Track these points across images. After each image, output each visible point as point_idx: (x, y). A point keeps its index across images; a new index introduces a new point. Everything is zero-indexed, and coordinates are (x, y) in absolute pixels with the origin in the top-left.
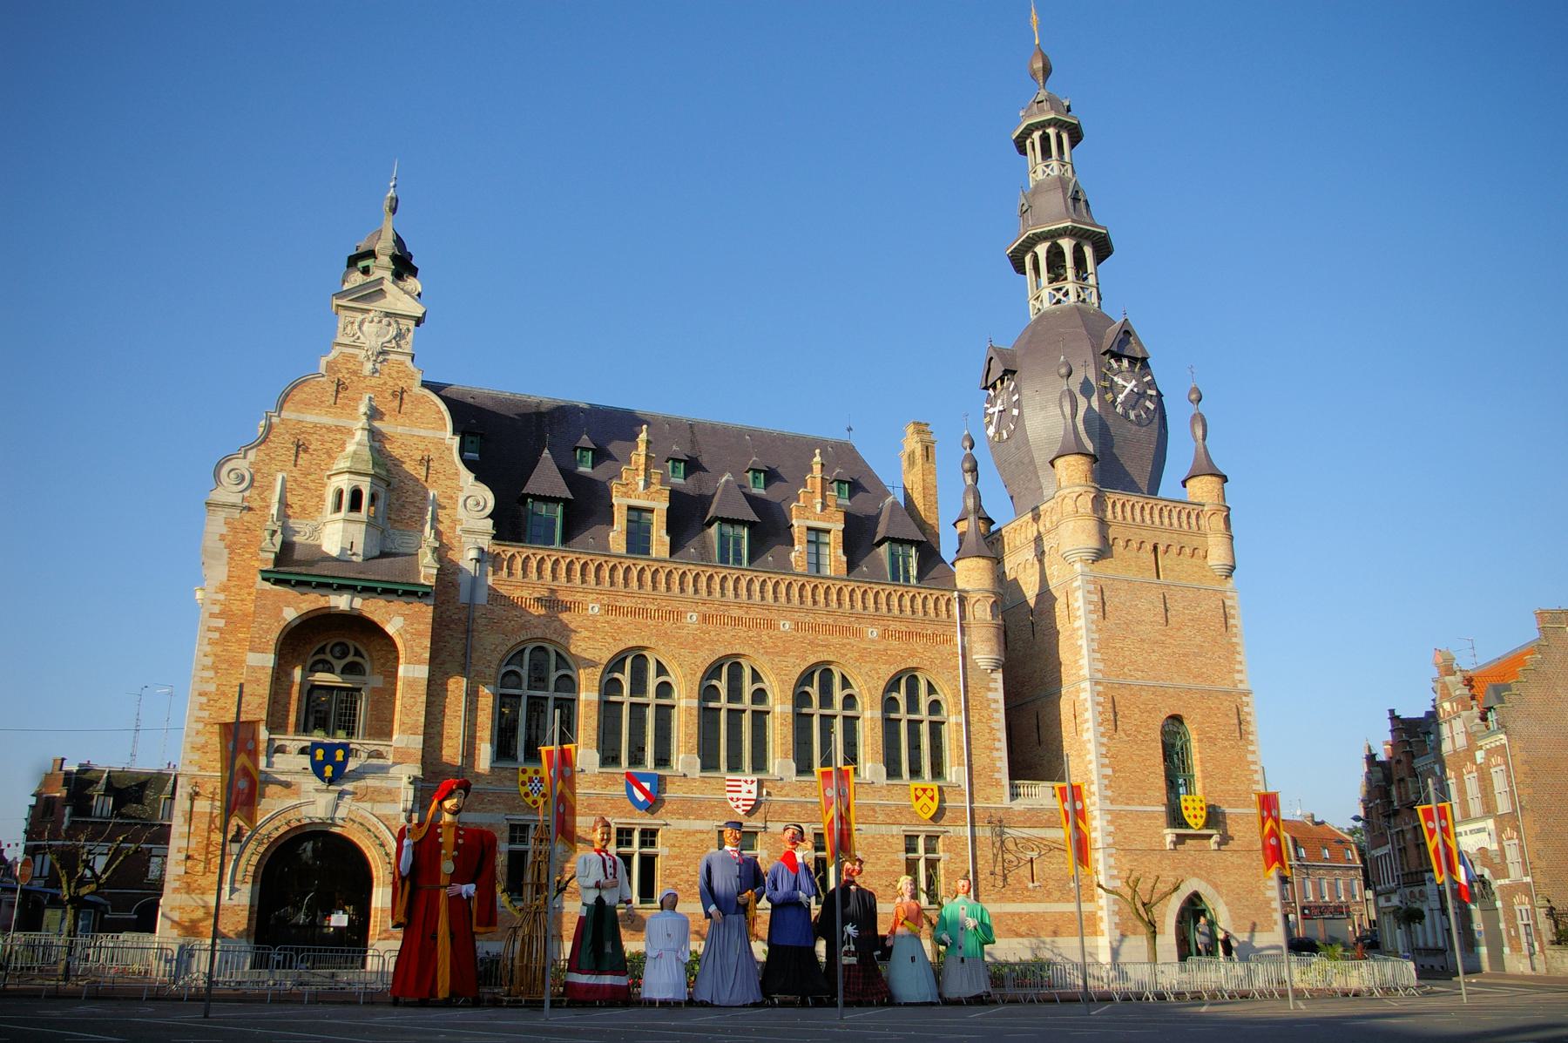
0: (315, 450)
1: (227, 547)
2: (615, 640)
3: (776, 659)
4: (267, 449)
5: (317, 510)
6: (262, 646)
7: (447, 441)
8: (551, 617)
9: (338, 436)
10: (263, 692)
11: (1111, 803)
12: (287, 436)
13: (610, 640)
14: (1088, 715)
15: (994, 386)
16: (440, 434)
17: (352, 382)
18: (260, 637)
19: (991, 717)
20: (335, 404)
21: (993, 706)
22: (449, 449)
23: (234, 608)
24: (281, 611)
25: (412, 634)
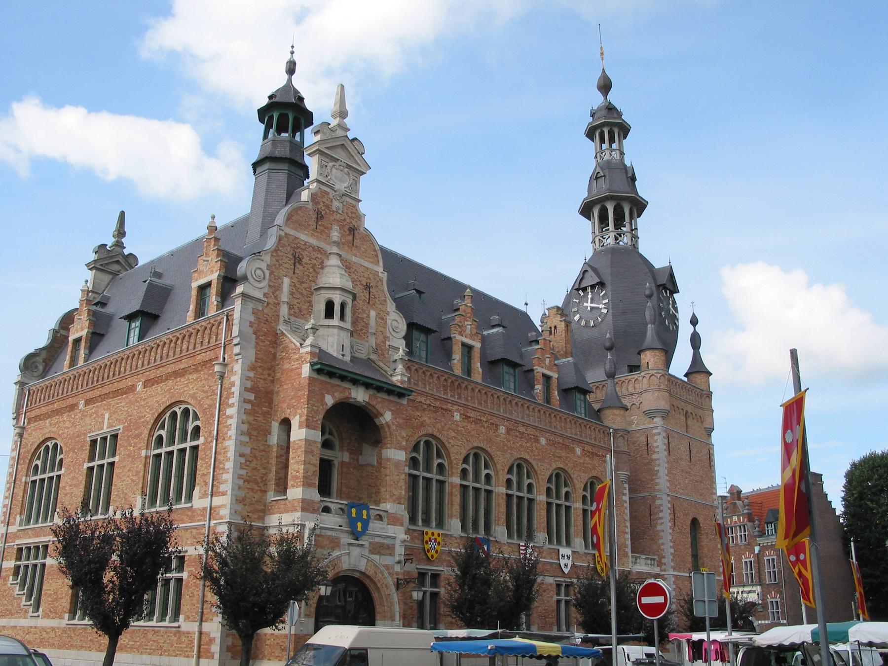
0: (306, 264)
1: (255, 333)
2: (467, 440)
3: (539, 464)
4: (277, 256)
5: (308, 314)
6: (313, 424)
7: (380, 275)
8: (436, 419)
9: (319, 256)
10: (315, 462)
11: (674, 571)
12: (289, 248)
13: (465, 441)
14: (229, 465)
15: (584, 289)
16: (376, 268)
17: (326, 213)
18: (312, 417)
19: (624, 513)
20: (316, 229)
21: (625, 505)
22: (381, 280)
23: (260, 385)
24: (324, 397)
25: (396, 426)
